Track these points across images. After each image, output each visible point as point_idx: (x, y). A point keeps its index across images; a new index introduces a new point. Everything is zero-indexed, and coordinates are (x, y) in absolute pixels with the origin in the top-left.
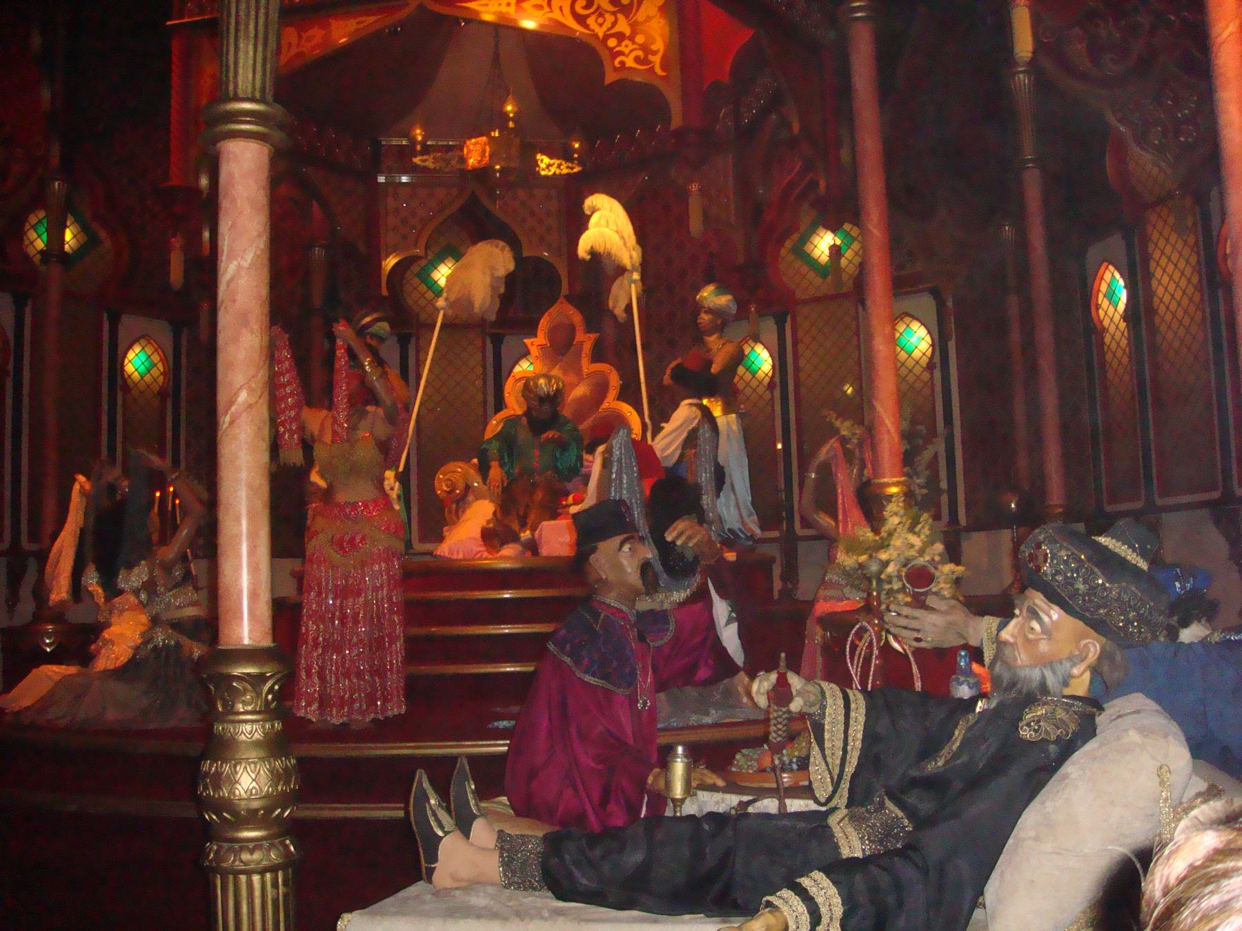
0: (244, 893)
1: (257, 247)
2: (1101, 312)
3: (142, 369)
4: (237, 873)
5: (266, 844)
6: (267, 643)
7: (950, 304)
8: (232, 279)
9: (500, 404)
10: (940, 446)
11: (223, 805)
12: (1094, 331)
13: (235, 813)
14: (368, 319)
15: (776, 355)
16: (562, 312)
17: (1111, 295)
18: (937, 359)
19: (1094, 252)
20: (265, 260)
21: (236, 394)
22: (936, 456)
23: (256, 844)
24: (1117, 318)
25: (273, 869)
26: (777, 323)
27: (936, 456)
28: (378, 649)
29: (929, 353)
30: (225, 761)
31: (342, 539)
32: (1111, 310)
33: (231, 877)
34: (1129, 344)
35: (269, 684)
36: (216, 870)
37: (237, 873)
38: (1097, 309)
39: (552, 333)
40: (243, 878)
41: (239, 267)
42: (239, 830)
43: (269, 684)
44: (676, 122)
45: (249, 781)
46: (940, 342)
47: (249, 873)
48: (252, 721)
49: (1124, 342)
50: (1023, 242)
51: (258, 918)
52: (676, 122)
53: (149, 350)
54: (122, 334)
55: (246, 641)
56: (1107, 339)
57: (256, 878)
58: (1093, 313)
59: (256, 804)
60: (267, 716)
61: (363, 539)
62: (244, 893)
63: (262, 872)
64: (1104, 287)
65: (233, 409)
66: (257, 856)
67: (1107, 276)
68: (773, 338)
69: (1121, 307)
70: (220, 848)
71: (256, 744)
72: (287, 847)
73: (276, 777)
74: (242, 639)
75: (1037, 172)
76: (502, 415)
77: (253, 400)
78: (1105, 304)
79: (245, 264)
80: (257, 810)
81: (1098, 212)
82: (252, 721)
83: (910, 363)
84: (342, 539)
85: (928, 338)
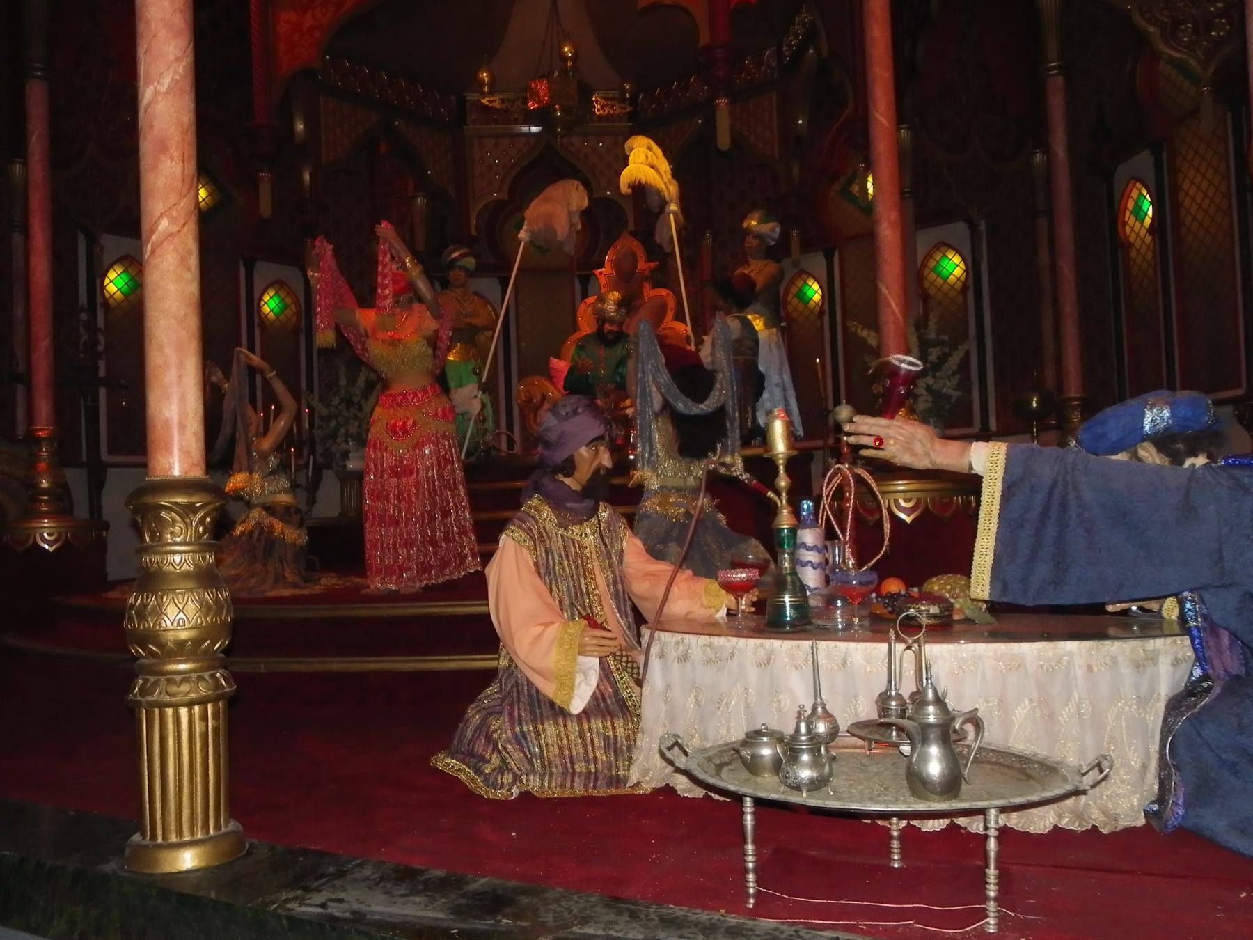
0: (170, 726)
1: (175, 72)
2: (1128, 229)
3: (277, 310)
4: (162, 706)
5: (194, 676)
6: (198, 473)
7: (983, 227)
8: (149, 105)
9: (575, 327)
10: (972, 346)
11: (147, 638)
12: (1120, 245)
13: (161, 645)
14: (456, 255)
15: (825, 286)
16: (626, 244)
17: (1138, 208)
18: (970, 283)
19: (1122, 172)
20: (188, 85)
21: (157, 223)
22: (967, 353)
23: (185, 677)
24: (1143, 232)
25: (203, 702)
26: (826, 257)
27: (967, 353)
28: (430, 521)
29: (963, 278)
30: (154, 592)
31: (395, 424)
32: (1138, 225)
33: (157, 710)
34: (1154, 256)
35: (199, 516)
36: (139, 704)
37: (162, 706)
38: (1124, 227)
39: (617, 265)
40: (169, 711)
41: (156, 93)
42: (165, 663)
43: (199, 516)
44: (704, 39)
45: (180, 616)
46: (973, 268)
47: (176, 706)
48: (181, 552)
49: (1149, 255)
50: (1049, 164)
51: (185, 752)
52: (704, 39)
53: (282, 293)
54: (258, 284)
55: (176, 472)
56: (1133, 254)
57: (183, 711)
58: (1120, 228)
59: (184, 635)
60: (196, 548)
61: (415, 424)
62: (170, 726)
63: (190, 705)
64: (1131, 205)
65: (154, 237)
66: (185, 688)
67: (1135, 194)
68: (824, 276)
69: (1148, 221)
70: (146, 681)
71: (186, 576)
72: (217, 680)
73: (205, 608)
74: (171, 467)
75: (1060, 79)
76: (576, 336)
77: (175, 229)
78: (1132, 221)
79: (163, 88)
80: (186, 641)
81: (1124, 131)
82: (181, 552)
83: (946, 288)
84: (395, 424)
85: (962, 265)
